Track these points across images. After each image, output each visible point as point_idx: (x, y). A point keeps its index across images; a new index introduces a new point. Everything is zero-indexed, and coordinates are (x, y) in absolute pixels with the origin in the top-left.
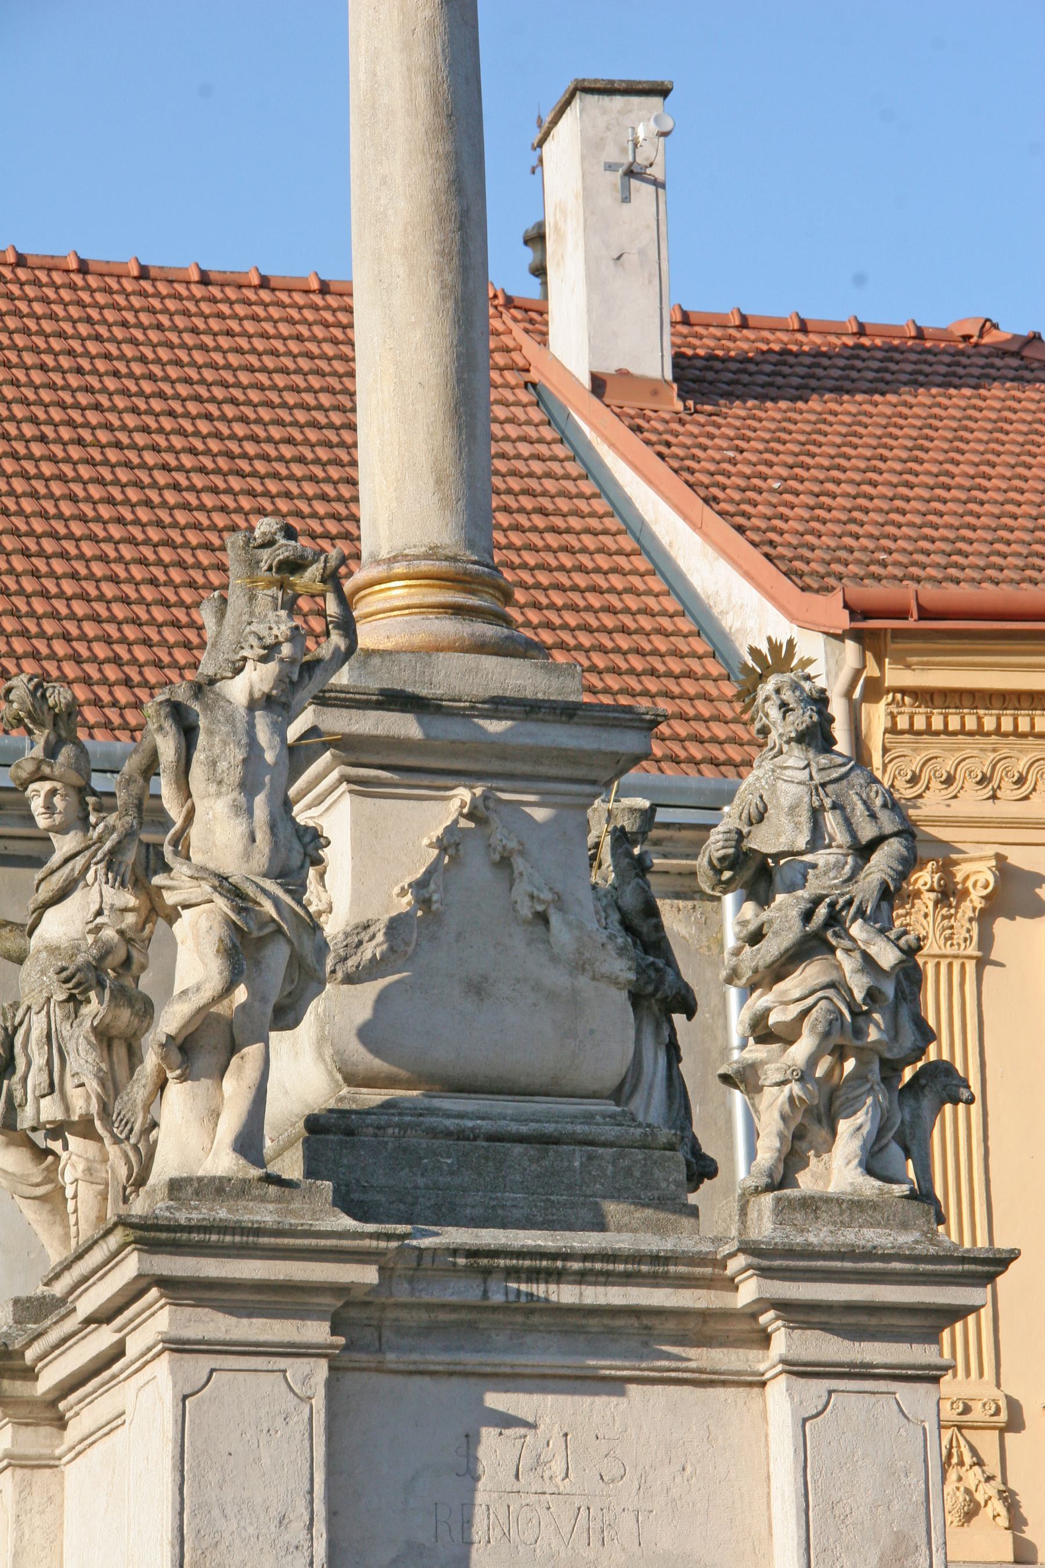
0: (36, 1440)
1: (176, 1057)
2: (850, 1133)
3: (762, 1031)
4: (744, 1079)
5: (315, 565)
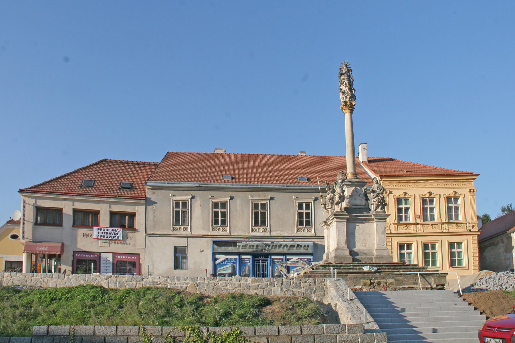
0: (328, 227)
2: (380, 207)
3: (374, 201)
4: (373, 204)
5: (344, 173)
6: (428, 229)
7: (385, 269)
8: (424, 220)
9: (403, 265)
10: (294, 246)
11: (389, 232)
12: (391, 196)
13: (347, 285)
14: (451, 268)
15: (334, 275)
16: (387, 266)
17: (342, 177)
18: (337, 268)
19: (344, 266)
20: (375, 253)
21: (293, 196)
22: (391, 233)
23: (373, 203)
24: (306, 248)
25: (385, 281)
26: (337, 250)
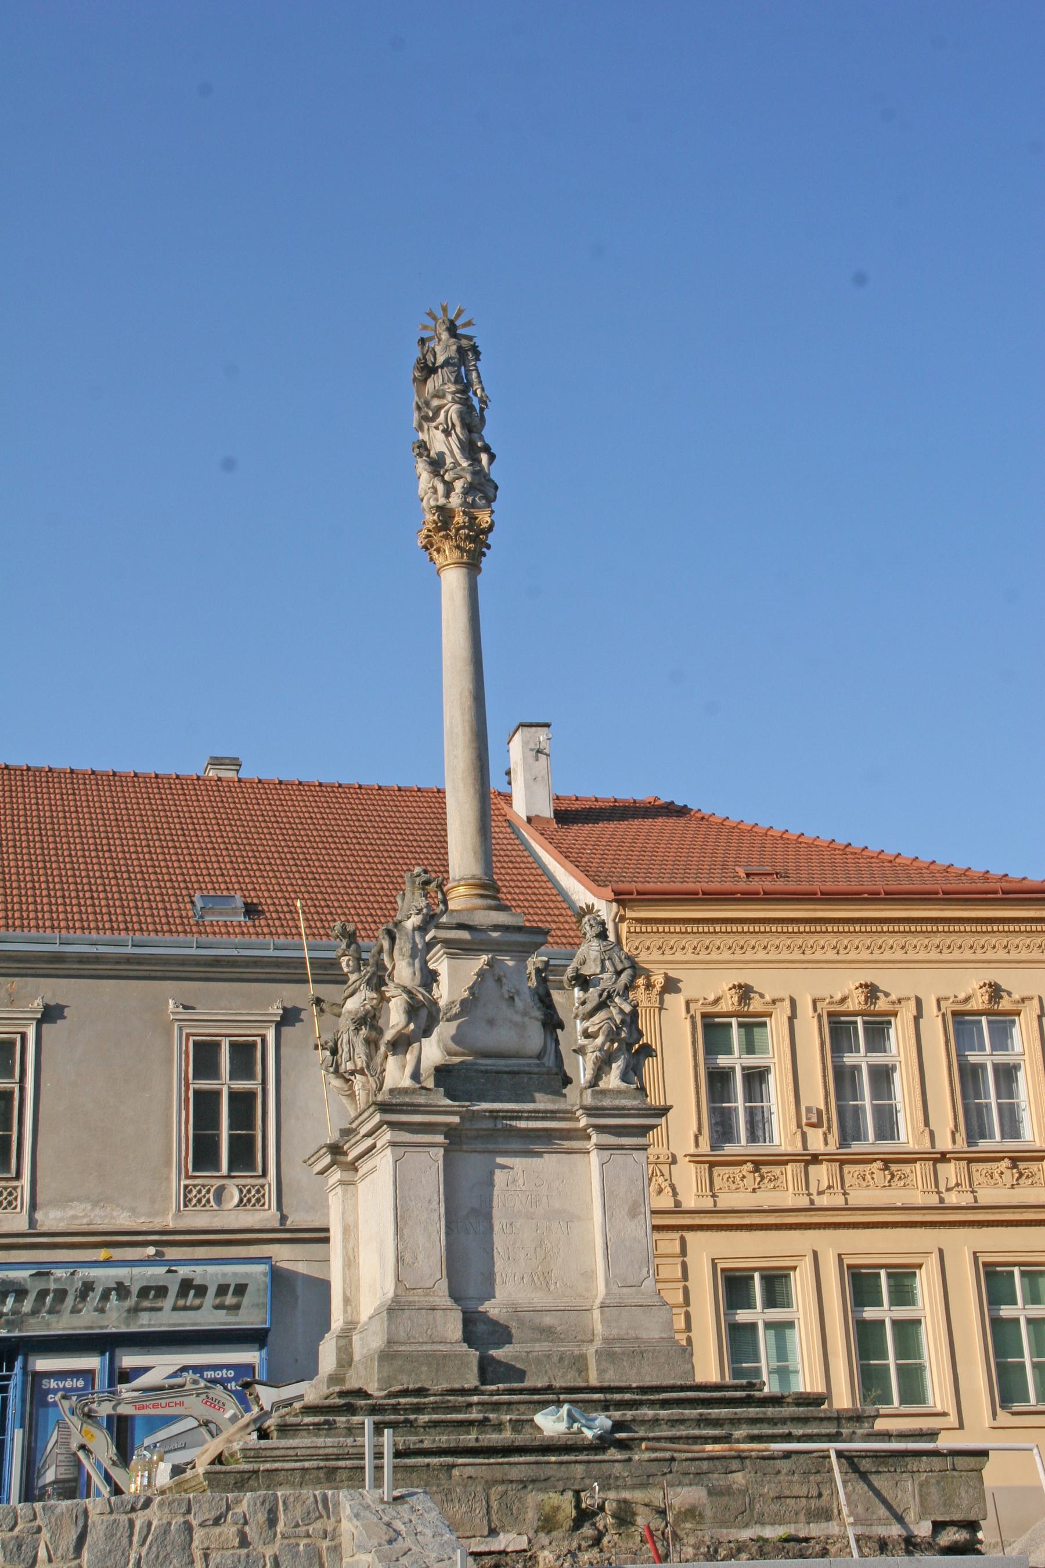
0: (348, 1176)
1: (391, 1048)
2: (617, 1067)
3: (587, 1035)
5: (434, 882)
6: (869, 1190)
7: (656, 1422)
8: (844, 1141)
9: (748, 1402)
10: (162, 1291)
11: (666, 1202)
12: (675, 1002)
13: (452, 1527)
14: (1004, 1418)
15: (379, 1468)
16: (665, 1404)
17: (422, 903)
18: (393, 1425)
19: (436, 1408)
20: (599, 1328)
21: (169, 997)
22: (678, 1210)
23: (582, 1041)
24: (230, 1300)
25: (655, 1496)
26: (394, 1309)
